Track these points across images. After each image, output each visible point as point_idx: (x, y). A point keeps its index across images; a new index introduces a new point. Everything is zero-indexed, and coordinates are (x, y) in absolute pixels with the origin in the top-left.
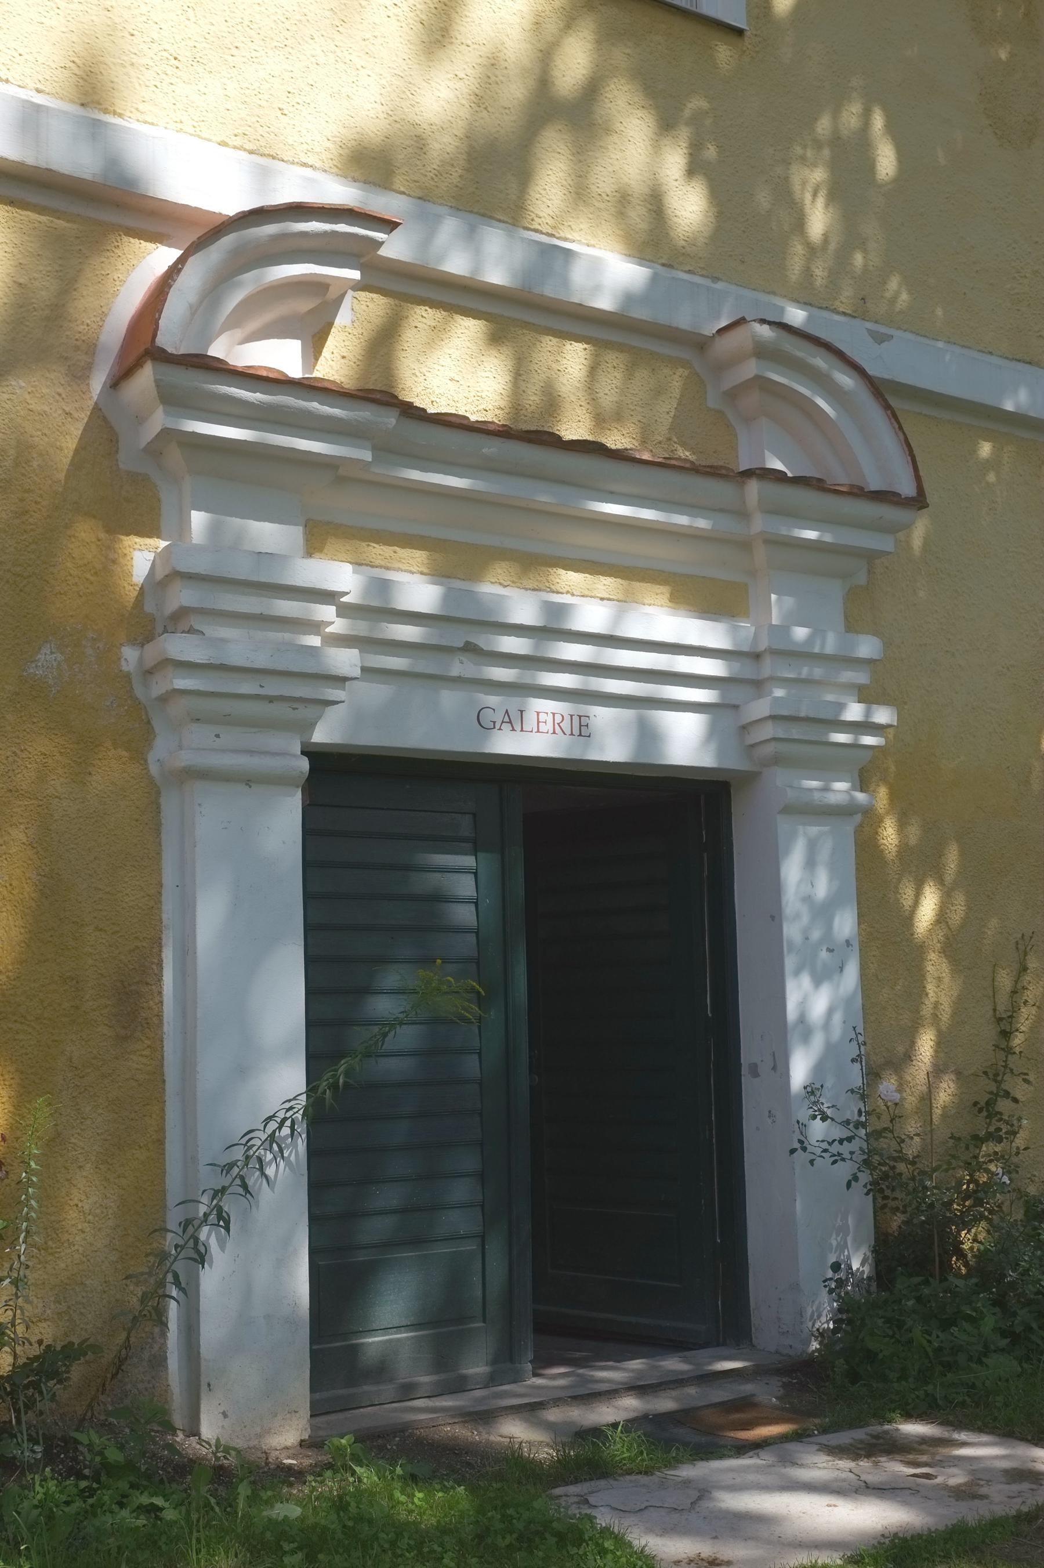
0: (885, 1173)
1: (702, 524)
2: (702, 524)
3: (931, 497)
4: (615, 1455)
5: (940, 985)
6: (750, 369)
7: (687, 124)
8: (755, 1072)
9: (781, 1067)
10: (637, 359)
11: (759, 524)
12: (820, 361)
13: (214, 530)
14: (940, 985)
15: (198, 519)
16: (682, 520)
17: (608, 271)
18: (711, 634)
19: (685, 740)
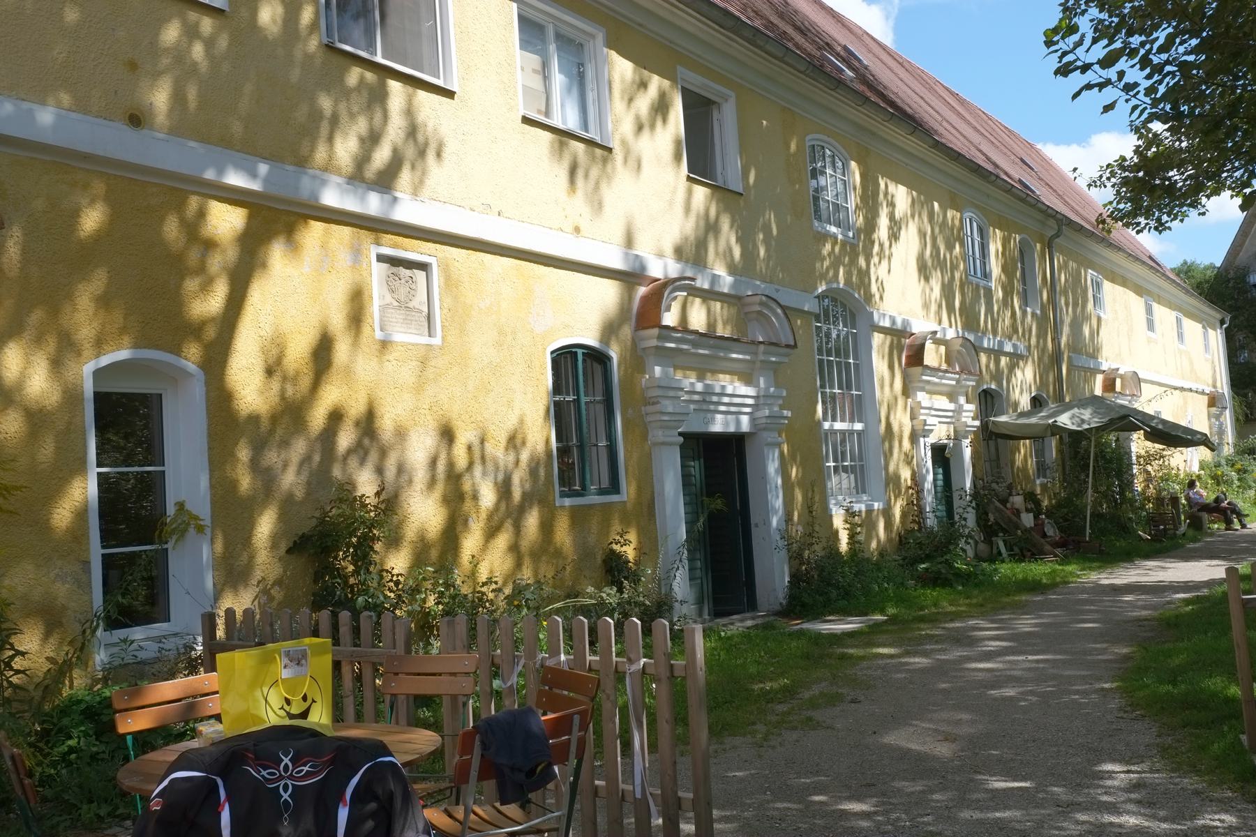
0: (796, 557)
1: (748, 357)
2: (748, 357)
3: (799, 344)
4: (339, 524)
5: (799, 496)
6: (758, 308)
7: (1229, 570)
8: (757, 525)
9: (767, 522)
10: (729, 304)
11: (762, 357)
12: (774, 306)
13: (665, 374)
14: (799, 496)
15: (658, 370)
16: (741, 356)
17: (726, 281)
18: (750, 391)
19: (745, 424)
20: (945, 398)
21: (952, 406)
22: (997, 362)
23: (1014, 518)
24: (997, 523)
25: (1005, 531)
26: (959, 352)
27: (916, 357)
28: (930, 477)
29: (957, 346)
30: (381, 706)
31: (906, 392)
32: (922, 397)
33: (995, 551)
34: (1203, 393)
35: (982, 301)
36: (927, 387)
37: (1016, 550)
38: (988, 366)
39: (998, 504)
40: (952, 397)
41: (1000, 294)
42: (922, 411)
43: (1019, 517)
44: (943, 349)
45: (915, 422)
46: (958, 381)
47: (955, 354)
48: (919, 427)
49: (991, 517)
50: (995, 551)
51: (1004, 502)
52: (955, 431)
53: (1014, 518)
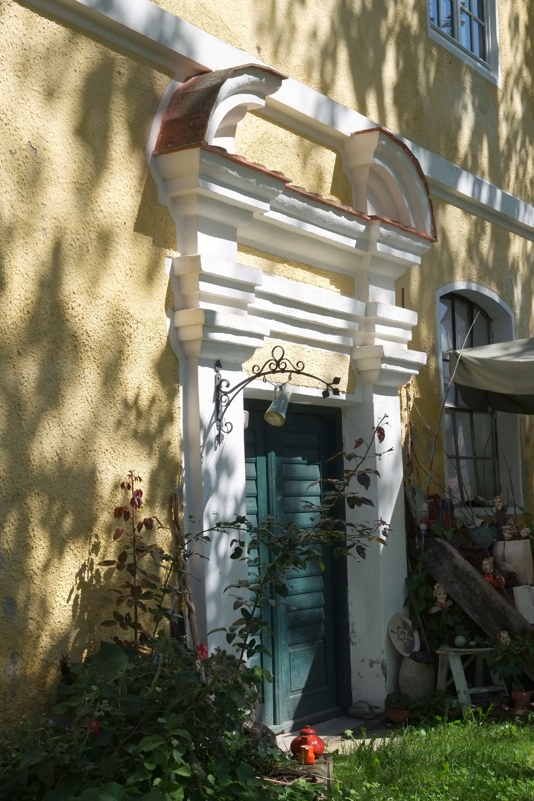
20: (325, 282)
21: (343, 303)
22: (501, 244)
23: (498, 599)
24: (454, 608)
25: (474, 631)
26: (373, 171)
27: (188, 118)
28: (237, 483)
29: (366, 155)
30: (409, 403)
31: (157, 220)
32: (215, 253)
33: (442, 684)
34: (198, 324)
35: (468, 98)
36: (245, 232)
37: (499, 683)
38: (473, 246)
39: (459, 559)
40: (350, 283)
41: (518, 107)
42: (204, 287)
43: (511, 598)
44: (327, 159)
45: (183, 318)
46: (364, 242)
47: (364, 177)
48: (192, 333)
49: (440, 593)
50: (442, 684)
51: (476, 553)
52: (355, 372)
53: (498, 599)
